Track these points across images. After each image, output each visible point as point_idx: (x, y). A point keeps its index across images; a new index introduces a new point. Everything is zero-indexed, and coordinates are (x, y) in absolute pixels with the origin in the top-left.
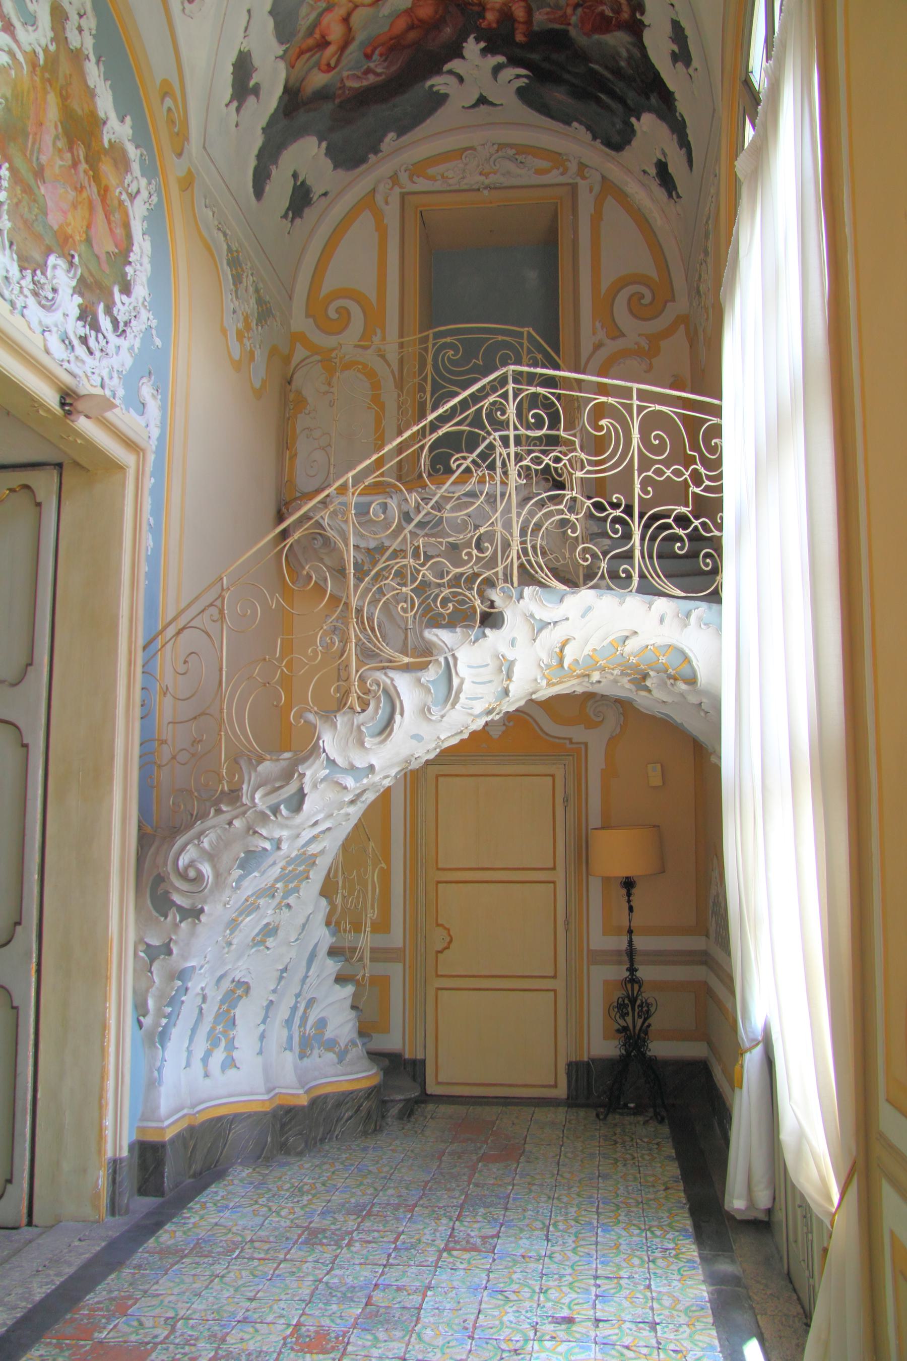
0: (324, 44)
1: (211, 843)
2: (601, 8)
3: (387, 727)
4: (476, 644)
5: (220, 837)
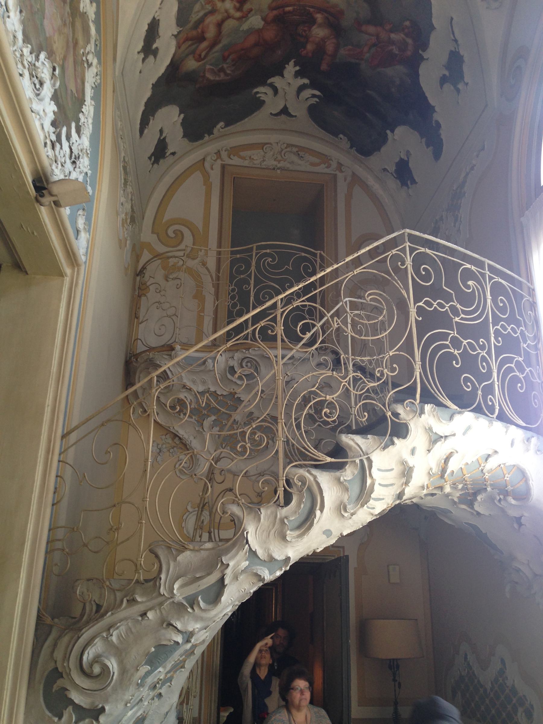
0: (201, 38)
1: (119, 636)
2: (391, 48)
3: (306, 522)
4: (386, 450)
5: (130, 629)
